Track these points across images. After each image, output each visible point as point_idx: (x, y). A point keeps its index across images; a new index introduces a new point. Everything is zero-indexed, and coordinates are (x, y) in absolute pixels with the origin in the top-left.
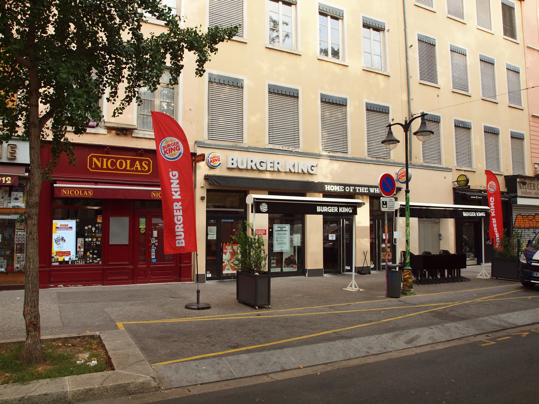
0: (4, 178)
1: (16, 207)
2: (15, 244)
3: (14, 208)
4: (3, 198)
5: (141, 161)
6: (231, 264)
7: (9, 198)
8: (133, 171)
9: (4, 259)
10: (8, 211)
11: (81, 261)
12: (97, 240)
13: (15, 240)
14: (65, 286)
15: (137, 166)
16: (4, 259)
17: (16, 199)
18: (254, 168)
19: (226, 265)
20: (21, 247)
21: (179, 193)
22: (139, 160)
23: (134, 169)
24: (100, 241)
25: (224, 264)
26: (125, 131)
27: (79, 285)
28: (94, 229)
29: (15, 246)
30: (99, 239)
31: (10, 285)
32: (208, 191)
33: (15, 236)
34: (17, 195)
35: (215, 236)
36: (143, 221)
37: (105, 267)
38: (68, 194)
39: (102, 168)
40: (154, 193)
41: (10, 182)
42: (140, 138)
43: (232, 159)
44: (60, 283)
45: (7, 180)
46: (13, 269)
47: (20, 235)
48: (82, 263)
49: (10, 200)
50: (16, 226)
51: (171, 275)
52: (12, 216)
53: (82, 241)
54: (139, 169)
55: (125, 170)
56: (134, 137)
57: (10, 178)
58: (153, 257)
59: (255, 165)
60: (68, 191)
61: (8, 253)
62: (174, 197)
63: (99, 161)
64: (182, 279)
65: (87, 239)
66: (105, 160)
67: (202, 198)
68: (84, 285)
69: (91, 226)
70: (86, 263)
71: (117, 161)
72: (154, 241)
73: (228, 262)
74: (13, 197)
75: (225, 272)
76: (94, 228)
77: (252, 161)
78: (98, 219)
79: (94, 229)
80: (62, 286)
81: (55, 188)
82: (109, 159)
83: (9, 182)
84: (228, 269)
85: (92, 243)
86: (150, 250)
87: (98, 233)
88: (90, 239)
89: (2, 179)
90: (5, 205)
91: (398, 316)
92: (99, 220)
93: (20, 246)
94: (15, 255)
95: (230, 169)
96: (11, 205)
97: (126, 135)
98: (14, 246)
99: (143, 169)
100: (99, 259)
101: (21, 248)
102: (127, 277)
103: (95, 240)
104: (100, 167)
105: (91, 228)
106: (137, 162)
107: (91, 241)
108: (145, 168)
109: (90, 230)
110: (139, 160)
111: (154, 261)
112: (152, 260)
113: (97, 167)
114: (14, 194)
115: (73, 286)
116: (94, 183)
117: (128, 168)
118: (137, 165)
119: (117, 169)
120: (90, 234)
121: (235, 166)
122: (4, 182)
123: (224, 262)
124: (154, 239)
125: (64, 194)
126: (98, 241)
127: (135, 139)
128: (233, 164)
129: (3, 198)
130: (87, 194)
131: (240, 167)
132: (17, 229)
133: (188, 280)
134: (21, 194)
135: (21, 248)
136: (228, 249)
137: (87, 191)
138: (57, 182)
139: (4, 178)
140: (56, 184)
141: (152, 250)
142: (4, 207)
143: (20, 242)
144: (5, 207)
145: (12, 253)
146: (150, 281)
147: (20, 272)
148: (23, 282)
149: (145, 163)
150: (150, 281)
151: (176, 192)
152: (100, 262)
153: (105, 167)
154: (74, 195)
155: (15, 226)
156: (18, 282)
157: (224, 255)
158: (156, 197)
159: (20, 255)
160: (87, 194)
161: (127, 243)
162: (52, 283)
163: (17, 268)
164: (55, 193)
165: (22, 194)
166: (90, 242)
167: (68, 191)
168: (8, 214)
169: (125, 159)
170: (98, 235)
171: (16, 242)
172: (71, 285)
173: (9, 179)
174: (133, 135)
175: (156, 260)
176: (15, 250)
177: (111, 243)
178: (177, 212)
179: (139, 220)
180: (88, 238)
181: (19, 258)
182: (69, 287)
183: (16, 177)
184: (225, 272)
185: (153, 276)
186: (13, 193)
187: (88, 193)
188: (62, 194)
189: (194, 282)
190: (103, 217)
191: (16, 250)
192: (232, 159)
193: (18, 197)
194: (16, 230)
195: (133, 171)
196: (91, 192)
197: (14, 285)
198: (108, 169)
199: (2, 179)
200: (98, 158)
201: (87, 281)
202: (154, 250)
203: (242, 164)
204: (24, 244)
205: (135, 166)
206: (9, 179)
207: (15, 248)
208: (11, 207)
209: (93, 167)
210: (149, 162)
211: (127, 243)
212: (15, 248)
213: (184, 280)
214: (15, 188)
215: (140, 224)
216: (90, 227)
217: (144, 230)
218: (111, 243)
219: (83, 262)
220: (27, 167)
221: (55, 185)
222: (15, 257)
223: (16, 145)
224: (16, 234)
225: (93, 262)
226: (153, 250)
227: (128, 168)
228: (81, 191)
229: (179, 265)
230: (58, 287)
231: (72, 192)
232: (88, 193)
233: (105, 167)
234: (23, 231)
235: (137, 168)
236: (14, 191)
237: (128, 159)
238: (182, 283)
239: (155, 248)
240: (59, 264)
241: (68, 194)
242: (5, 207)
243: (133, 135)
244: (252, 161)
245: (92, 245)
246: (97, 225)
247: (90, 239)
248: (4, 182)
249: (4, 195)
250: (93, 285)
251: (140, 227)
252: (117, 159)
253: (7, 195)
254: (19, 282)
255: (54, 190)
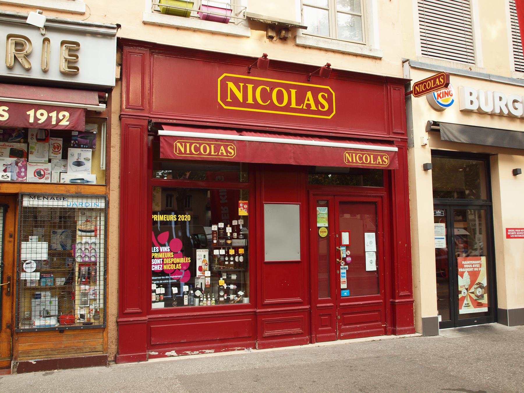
0: (55, 112)
1: (79, 181)
2: (77, 265)
3: (73, 183)
4: (50, 161)
5: (315, 92)
6: (471, 295)
7: (63, 163)
8: (301, 111)
9: (52, 296)
10: (62, 190)
11: (207, 298)
12: (237, 253)
13: (77, 255)
14: (180, 353)
15: (308, 102)
16: (52, 296)
17: (79, 164)
18: (506, 112)
19: (464, 298)
20: (89, 269)
21: (226, 197)
22: (313, 90)
23: (304, 107)
24: (243, 255)
25: (460, 296)
26: (284, 32)
27: (207, 351)
28: (229, 230)
29: (77, 269)
30: (241, 251)
31: (69, 356)
32: (434, 153)
33: (78, 247)
34: (79, 155)
35: (444, 241)
36: (322, 213)
37: (258, 311)
38: (188, 152)
39: (245, 104)
40: (349, 153)
41: (68, 123)
42: (310, 47)
43: (471, 94)
44: (170, 346)
45: (61, 117)
46: (73, 321)
47: (86, 243)
48: (209, 302)
49: (64, 166)
50: (79, 223)
51: (377, 321)
52: (70, 200)
53: (205, 256)
54: (313, 107)
55: (287, 108)
56: (298, 46)
57: (67, 114)
58: (344, 286)
59: (506, 105)
60: (188, 145)
61: (60, 281)
62: (221, 202)
63: (239, 88)
64: (398, 329)
65: (216, 252)
66: (250, 87)
67: (426, 168)
68: (218, 350)
69: (223, 224)
70: (217, 301)
71: (272, 90)
72: (344, 253)
73: (466, 291)
74: (71, 160)
75: (463, 311)
76: (231, 228)
77: (501, 99)
78: (239, 209)
79: (229, 230)
80: (173, 353)
81: (161, 139)
82: (256, 84)
83: (65, 123)
84: (468, 306)
85: (227, 259)
86: (338, 272)
87: (238, 238)
88: (223, 252)
89: (50, 115)
90: (56, 177)
91: (363, 304)
92: (243, 212)
93: (87, 268)
94: (77, 288)
95: (466, 112)
96: (67, 178)
97: (284, 40)
98: (73, 270)
99: (320, 108)
100: (241, 293)
101: (89, 273)
102: (298, 330)
103: (232, 252)
104: (241, 101)
105: (225, 229)
106: (309, 94)
107: (224, 256)
108: (323, 107)
109: (221, 234)
110: (313, 90)
111: (345, 293)
112: (343, 292)
113: (235, 101)
114: (74, 153)
115: (195, 352)
116: (235, 132)
117: (293, 105)
118: (308, 100)
119: (272, 106)
120: (222, 241)
121: (474, 107)
122: (54, 122)
123: (460, 292)
124: (344, 248)
125: (180, 152)
126: (239, 255)
127: (300, 50)
128: (472, 102)
129: (50, 161)
130: (225, 154)
131: (485, 109)
132: (80, 230)
133: (409, 330)
134: (87, 153)
135: (89, 273)
136: (465, 266)
137: (226, 147)
138: (163, 126)
139: (55, 112)
140: (163, 129)
141: (342, 271)
142: (52, 182)
143: (87, 259)
144: (55, 181)
145: (70, 281)
146: (339, 334)
147: (88, 326)
148: (95, 348)
149: (323, 96)
150: (339, 334)
151: (223, 196)
152: (246, 300)
153: (250, 101)
154: (200, 154)
155: (75, 223)
156: (85, 350)
157: (459, 277)
158: (352, 162)
159: (87, 287)
160: (225, 154)
161: (297, 257)
162: (153, 347)
163: (82, 316)
164: (161, 150)
165: (91, 153)
166: (222, 258)
167: (188, 145)
168: (63, 197)
169: (288, 88)
170: (237, 243)
171: (79, 260)
172: (193, 350)
173: (64, 116)
174: (299, 41)
175: (348, 291)
176: (77, 278)
177: (269, 257)
178: (224, 216)
179: (316, 211)
180: (219, 249)
181: (85, 294)
182: (187, 354)
183: (79, 111)
184: (463, 311)
185: (345, 325)
186: (71, 151)
187: (227, 151)
188: (176, 151)
189: (420, 335)
190: (249, 205)
191: (79, 278)
192: (471, 94)
193: (82, 159)
194: (79, 233)
195: (301, 111)
196: (234, 150)
197: (76, 356)
198: (256, 105)
199: (50, 115)
200: (236, 82)
201: (223, 340)
202: (345, 271)
203: (486, 104)
204: (95, 264)
205: (306, 102)
206: (64, 116)
207: (77, 274)
208: (68, 182)
209: (229, 100)
210: (330, 95)
211: (297, 257)
212: (77, 274)
213: (401, 330)
214: (75, 141)
215: (318, 220)
216: (221, 225)
217: (325, 232)
218: (269, 257)
219: (211, 300)
220: (101, 94)
221: (160, 132)
222: (77, 293)
223: (78, 44)
224: (78, 241)
225: (228, 300)
226: (343, 271)
227: (293, 105)
228: (212, 146)
229: (391, 300)
230: (166, 356)
231: (197, 149)
232: (227, 151)
233: (250, 101)
234: (93, 234)
235: (309, 106)
236: (74, 147)
237: (294, 87)
238: (398, 336)
239: (347, 267)
240: (165, 306)
241: (188, 152)
242: (55, 182)
243: (299, 41)
244: (501, 99)
245: (227, 263)
246: (235, 223)
247: (223, 252)
248: (54, 122)
249: (53, 155)
250: (234, 350)
251: (319, 225)
252: (273, 86)
253: (60, 156)
254: (88, 350)
255: (159, 140)
